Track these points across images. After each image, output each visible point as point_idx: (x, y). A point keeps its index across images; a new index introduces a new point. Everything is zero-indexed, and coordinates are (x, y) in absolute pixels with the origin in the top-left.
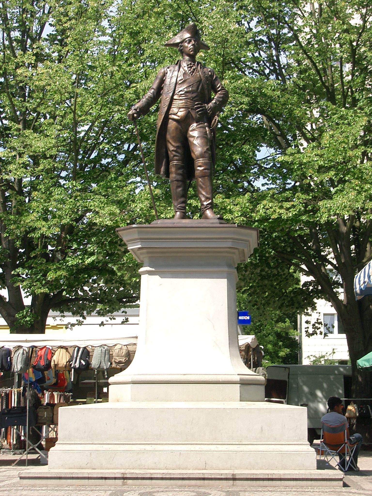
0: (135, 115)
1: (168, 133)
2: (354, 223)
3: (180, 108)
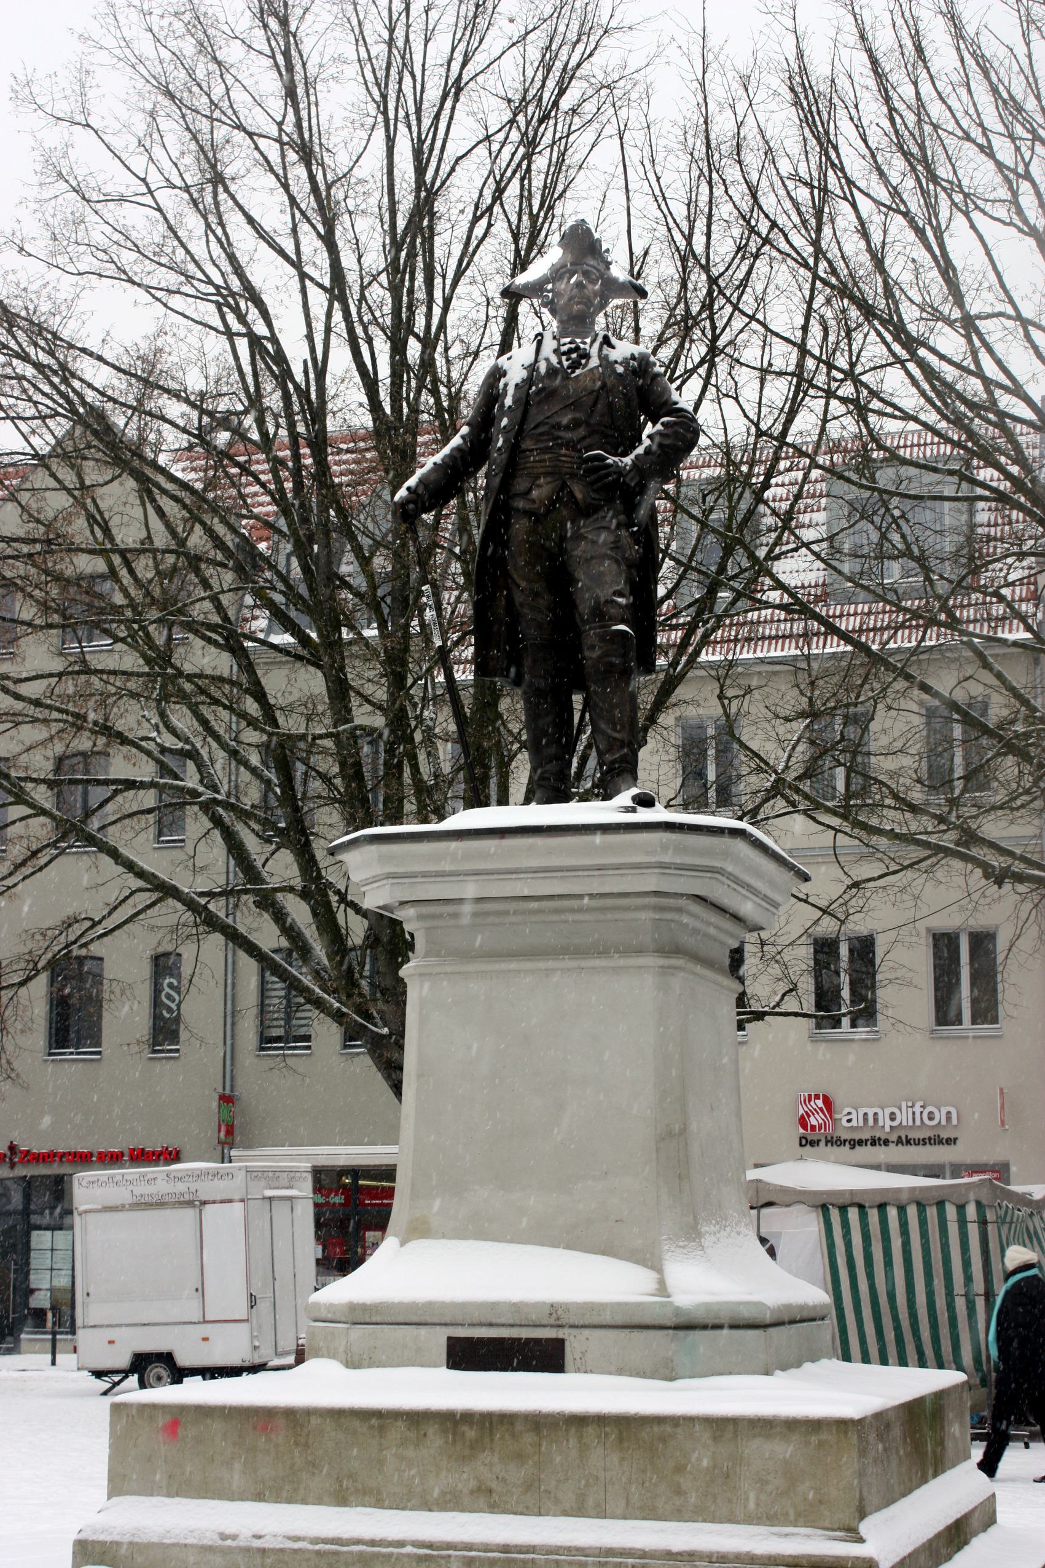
0: (411, 506)
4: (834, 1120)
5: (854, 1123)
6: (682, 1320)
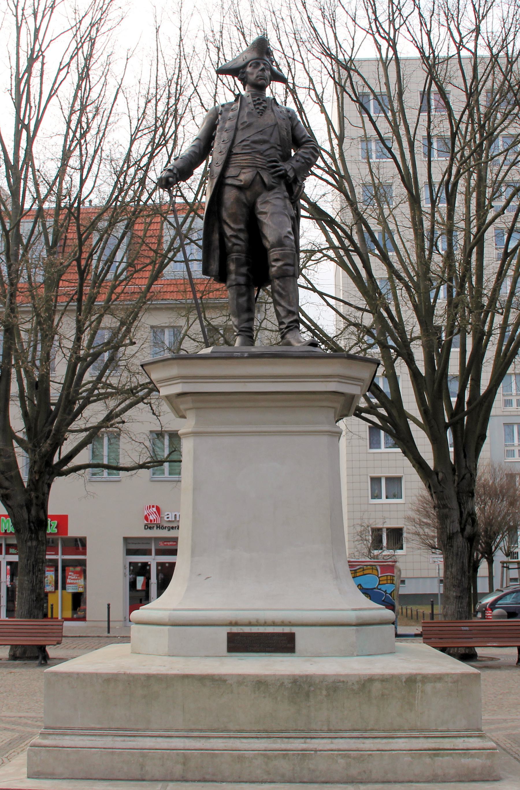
0: (171, 179)
1: (223, 209)
2: (71, 569)
3: (243, 167)
4: (161, 518)
5: (170, 519)
6: (360, 621)
